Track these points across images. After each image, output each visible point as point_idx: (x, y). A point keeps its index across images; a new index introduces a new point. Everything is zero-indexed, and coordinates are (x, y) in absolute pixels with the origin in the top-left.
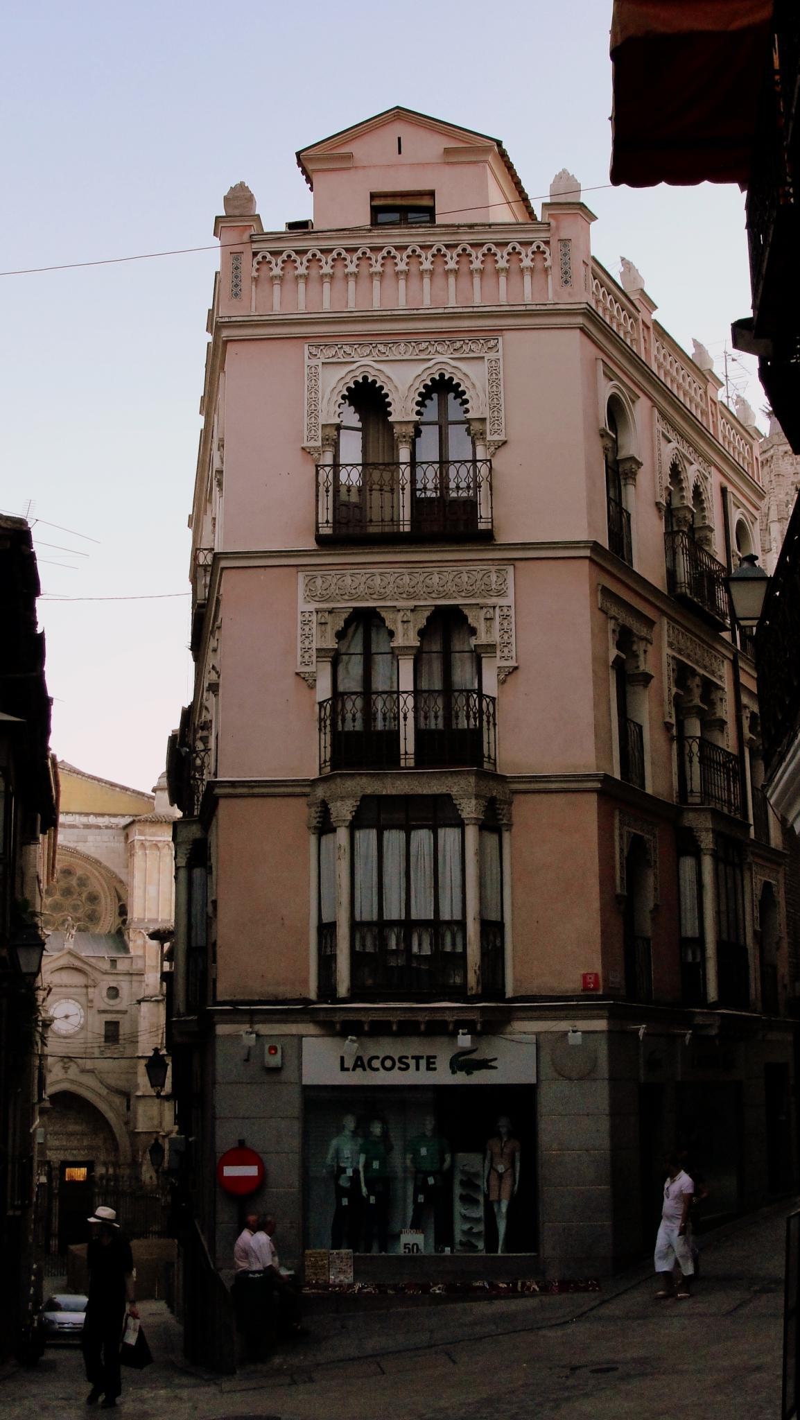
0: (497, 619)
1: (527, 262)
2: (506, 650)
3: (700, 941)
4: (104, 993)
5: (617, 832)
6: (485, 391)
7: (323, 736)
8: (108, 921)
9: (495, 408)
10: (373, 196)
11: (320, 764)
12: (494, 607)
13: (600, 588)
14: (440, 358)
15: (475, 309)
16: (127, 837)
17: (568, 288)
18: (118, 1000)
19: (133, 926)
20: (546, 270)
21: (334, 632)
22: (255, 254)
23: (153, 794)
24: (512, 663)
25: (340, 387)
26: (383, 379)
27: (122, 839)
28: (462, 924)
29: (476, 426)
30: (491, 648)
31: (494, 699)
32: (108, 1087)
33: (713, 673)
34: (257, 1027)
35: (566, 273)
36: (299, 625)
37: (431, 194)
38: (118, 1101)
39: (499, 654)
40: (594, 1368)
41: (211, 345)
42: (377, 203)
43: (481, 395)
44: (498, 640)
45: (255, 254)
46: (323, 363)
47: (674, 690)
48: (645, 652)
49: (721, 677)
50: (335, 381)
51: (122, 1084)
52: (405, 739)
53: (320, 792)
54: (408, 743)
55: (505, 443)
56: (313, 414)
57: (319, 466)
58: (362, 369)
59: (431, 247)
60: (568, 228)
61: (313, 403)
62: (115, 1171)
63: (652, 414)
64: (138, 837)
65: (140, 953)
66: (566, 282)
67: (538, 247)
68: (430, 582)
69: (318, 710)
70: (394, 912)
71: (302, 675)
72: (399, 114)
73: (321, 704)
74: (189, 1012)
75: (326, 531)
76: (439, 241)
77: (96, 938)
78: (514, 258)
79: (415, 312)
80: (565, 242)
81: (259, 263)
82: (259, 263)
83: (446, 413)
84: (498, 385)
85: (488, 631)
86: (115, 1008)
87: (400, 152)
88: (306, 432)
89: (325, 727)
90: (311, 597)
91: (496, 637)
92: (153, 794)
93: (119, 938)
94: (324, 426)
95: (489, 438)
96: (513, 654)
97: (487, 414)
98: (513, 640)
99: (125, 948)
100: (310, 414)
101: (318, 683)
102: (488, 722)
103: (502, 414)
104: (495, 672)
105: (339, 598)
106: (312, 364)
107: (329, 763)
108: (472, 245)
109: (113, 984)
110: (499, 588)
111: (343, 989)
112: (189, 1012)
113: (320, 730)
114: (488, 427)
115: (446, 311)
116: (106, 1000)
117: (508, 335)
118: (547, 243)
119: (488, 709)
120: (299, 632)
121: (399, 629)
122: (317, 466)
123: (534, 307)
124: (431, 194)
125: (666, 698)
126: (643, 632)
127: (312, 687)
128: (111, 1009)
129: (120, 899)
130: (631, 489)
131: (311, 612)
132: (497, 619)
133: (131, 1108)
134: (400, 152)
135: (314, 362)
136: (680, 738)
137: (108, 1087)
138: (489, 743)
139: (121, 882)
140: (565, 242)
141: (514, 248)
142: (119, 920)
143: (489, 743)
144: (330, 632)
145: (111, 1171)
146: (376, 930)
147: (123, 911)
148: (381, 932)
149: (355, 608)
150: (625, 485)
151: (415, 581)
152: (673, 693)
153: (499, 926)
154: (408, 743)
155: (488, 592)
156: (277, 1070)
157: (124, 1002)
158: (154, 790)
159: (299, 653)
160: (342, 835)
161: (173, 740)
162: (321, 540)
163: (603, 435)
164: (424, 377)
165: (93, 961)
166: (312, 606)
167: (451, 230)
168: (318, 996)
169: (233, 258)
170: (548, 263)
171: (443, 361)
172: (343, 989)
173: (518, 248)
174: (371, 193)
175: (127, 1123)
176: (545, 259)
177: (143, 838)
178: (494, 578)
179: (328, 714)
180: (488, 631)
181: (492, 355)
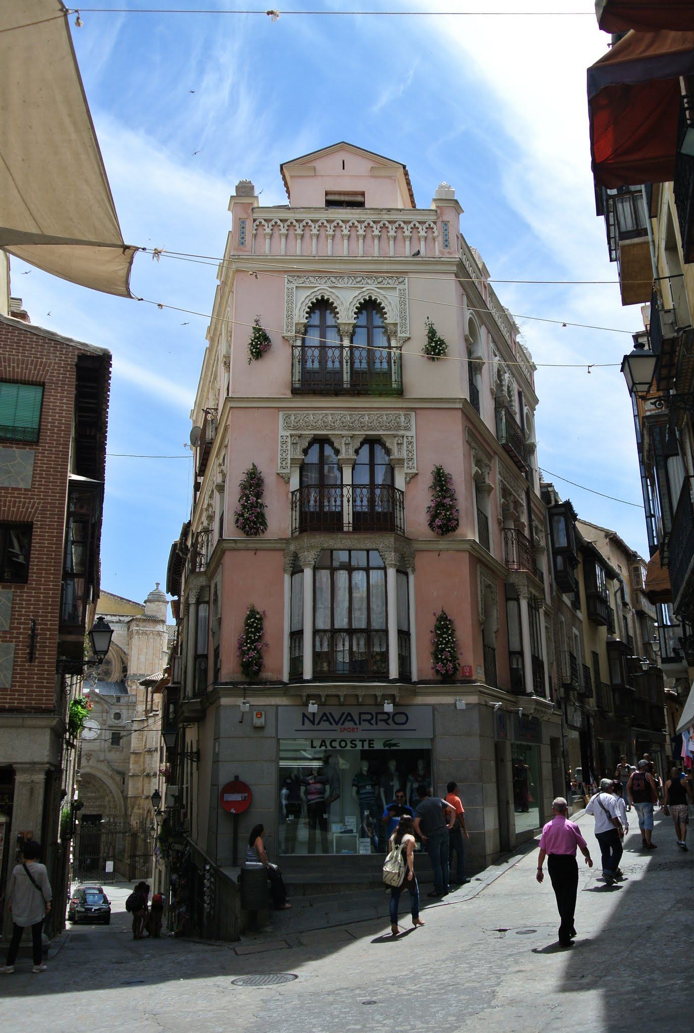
0: (405, 445)
1: (422, 233)
2: (410, 463)
3: (521, 653)
4: (112, 716)
5: (479, 580)
6: (397, 308)
7: (294, 512)
8: (116, 675)
9: (403, 318)
10: (327, 194)
11: (292, 531)
12: (403, 437)
13: (467, 428)
14: (369, 287)
15: (391, 259)
16: (129, 629)
17: (447, 250)
18: (120, 720)
19: (131, 678)
20: (434, 239)
21: (302, 449)
22: (255, 220)
23: (145, 604)
24: (415, 471)
25: (303, 307)
26: (334, 297)
27: (126, 629)
28: (386, 632)
29: (391, 328)
30: (401, 461)
31: (403, 492)
32: (113, 770)
33: (519, 496)
34: (248, 699)
35: (446, 241)
36: (280, 444)
37: (363, 194)
38: (118, 778)
39: (406, 465)
40: (518, 930)
41: (219, 287)
42: (330, 198)
43: (395, 309)
44: (405, 457)
45: (255, 220)
46: (296, 287)
47: (502, 500)
48: (489, 473)
49: (522, 499)
50: (303, 299)
51: (120, 769)
52: (349, 514)
53: (292, 548)
54: (348, 518)
55: (409, 338)
56: (290, 316)
57: (294, 346)
58: (320, 292)
59: (364, 222)
60: (448, 216)
61: (290, 310)
62: (114, 820)
63: (488, 338)
64: (135, 628)
65: (134, 693)
66: (447, 246)
67: (429, 225)
68: (363, 420)
69: (291, 497)
70: (342, 622)
71: (281, 475)
72: (343, 146)
73: (293, 493)
74: (194, 696)
75: (297, 386)
76: (369, 217)
77: (109, 684)
78: (415, 231)
79: (354, 258)
80: (446, 223)
81: (257, 226)
82: (257, 226)
83: (372, 320)
84: (405, 304)
85: (399, 450)
86: (118, 725)
87: (344, 169)
88: (285, 327)
89: (296, 507)
90: (287, 427)
91: (404, 454)
92: (145, 604)
93: (122, 685)
94: (297, 324)
95: (399, 335)
96: (415, 465)
97: (398, 321)
98: (415, 457)
99: (126, 692)
100: (288, 317)
101: (291, 480)
102: (400, 506)
103: (408, 321)
104: (404, 476)
105: (305, 428)
106: (290, 287)
107: (297, 530)
108: (389, 222)
109: (118, 711)
110: (407, 425)
111: (308, 674)
112: (194, 696)
113: (292, 509)
114: (399, 329)
115: (374, 259)
116: (113, 720)
117: (411, 275)
118: (435, 223)
119: (400, 498)
120: (280, 448)
121: (343, 449)
122: (293, 346)
123: (427, 259)
124: (363, 194)
125: (498, 506)
126: (487, 462)
127: (288, 482)
128: (116, 725)
129: (123, 663)
130: (479, 377)
131: (287, 436)
132: (405, 445)
133: (125, 783)
134: (344, 169)
135: (290, 286)
136: (504, 530)
137: (113, 770)
138: (400, 519)
139: (125, 653)
140: (446, 223)
141: (415, 225)
142: (122, 675)
143: (400, 519)
144: (299, 449)
145: (112, 820)
146: (329, 634)
147: (125, 670)
148: (332, 637)
149: (314, 435)
150: (475, 375)
151: (353, 420)
152: (502, 502)
153: (408, 634)
154: (348, 518)
155: (398, 427)
156: (261, 728)
157: (124, 721)
158: (145, 602)
159: (279, 461)
160: (308, 572)
161: (175, 546)
162: (295, 392)
163: (466, 340)
164: (359, 297)
165: (106, 698)
166: (288, 433)
167: (376, 212)
168: (290, 680)
169: (240, 225)
170: (435, 234)
171: (371, 290)
172: (308, 674)
173: (417, 225)
174: (326, 191)
175: (122, 792)
176: (434, 232)
177: (138, 628)
178: (403, 419)
179: (298, 499)
180: (399, 450)
181: (401, 287)
